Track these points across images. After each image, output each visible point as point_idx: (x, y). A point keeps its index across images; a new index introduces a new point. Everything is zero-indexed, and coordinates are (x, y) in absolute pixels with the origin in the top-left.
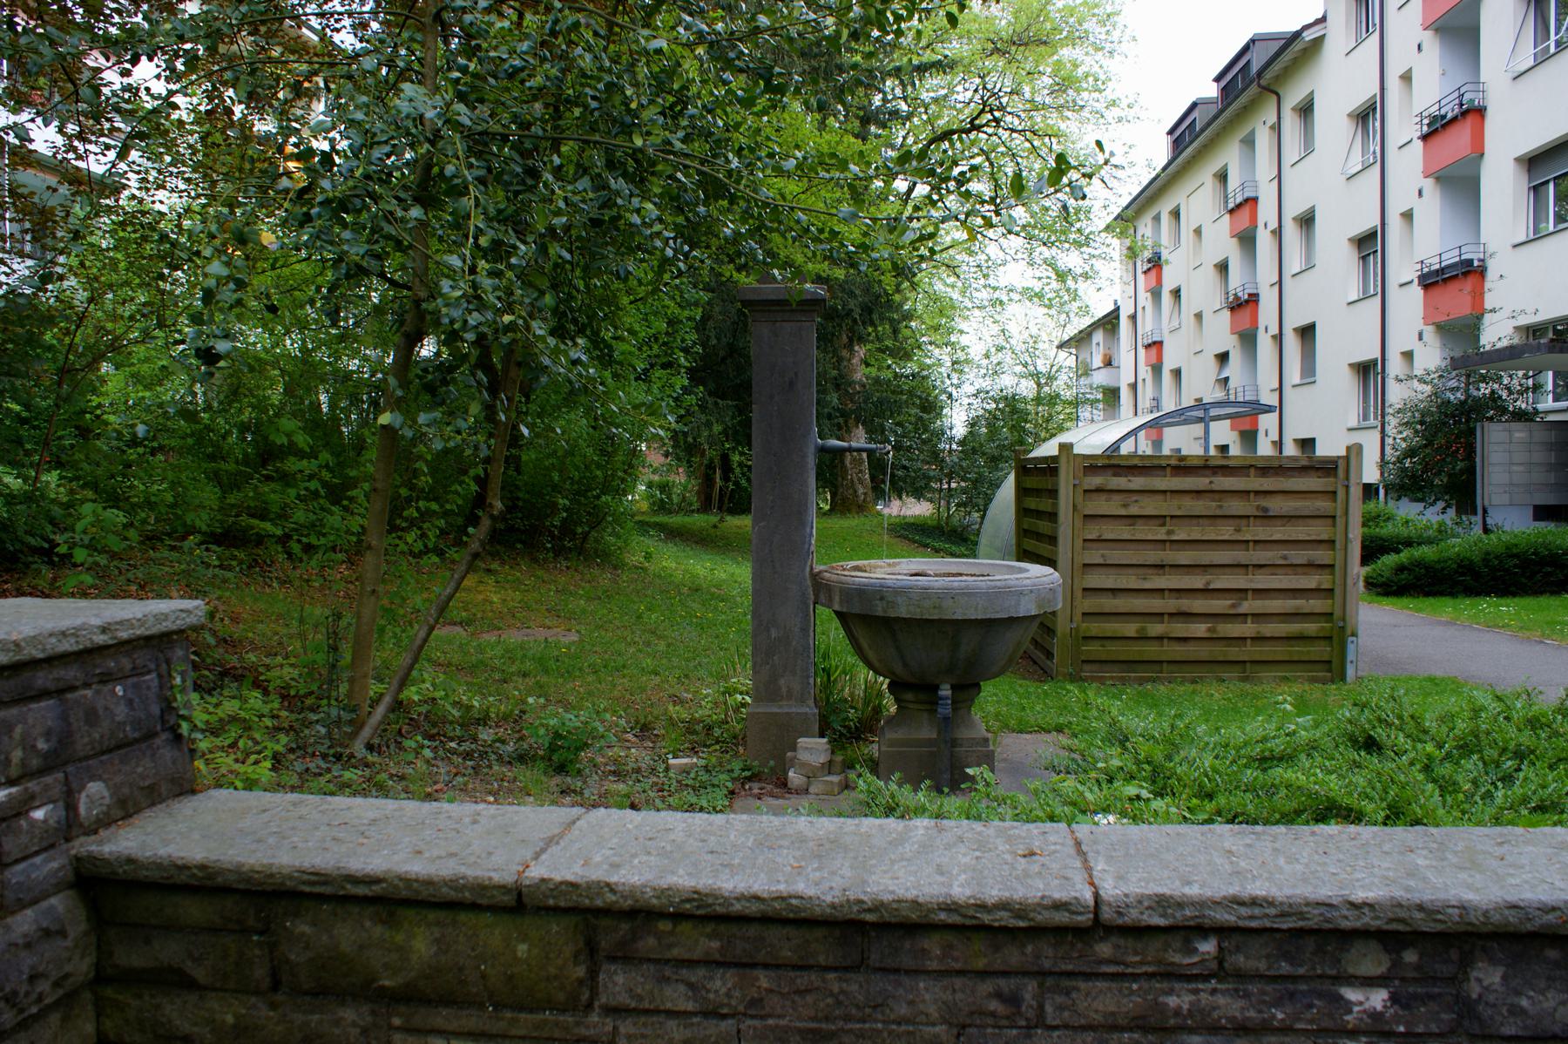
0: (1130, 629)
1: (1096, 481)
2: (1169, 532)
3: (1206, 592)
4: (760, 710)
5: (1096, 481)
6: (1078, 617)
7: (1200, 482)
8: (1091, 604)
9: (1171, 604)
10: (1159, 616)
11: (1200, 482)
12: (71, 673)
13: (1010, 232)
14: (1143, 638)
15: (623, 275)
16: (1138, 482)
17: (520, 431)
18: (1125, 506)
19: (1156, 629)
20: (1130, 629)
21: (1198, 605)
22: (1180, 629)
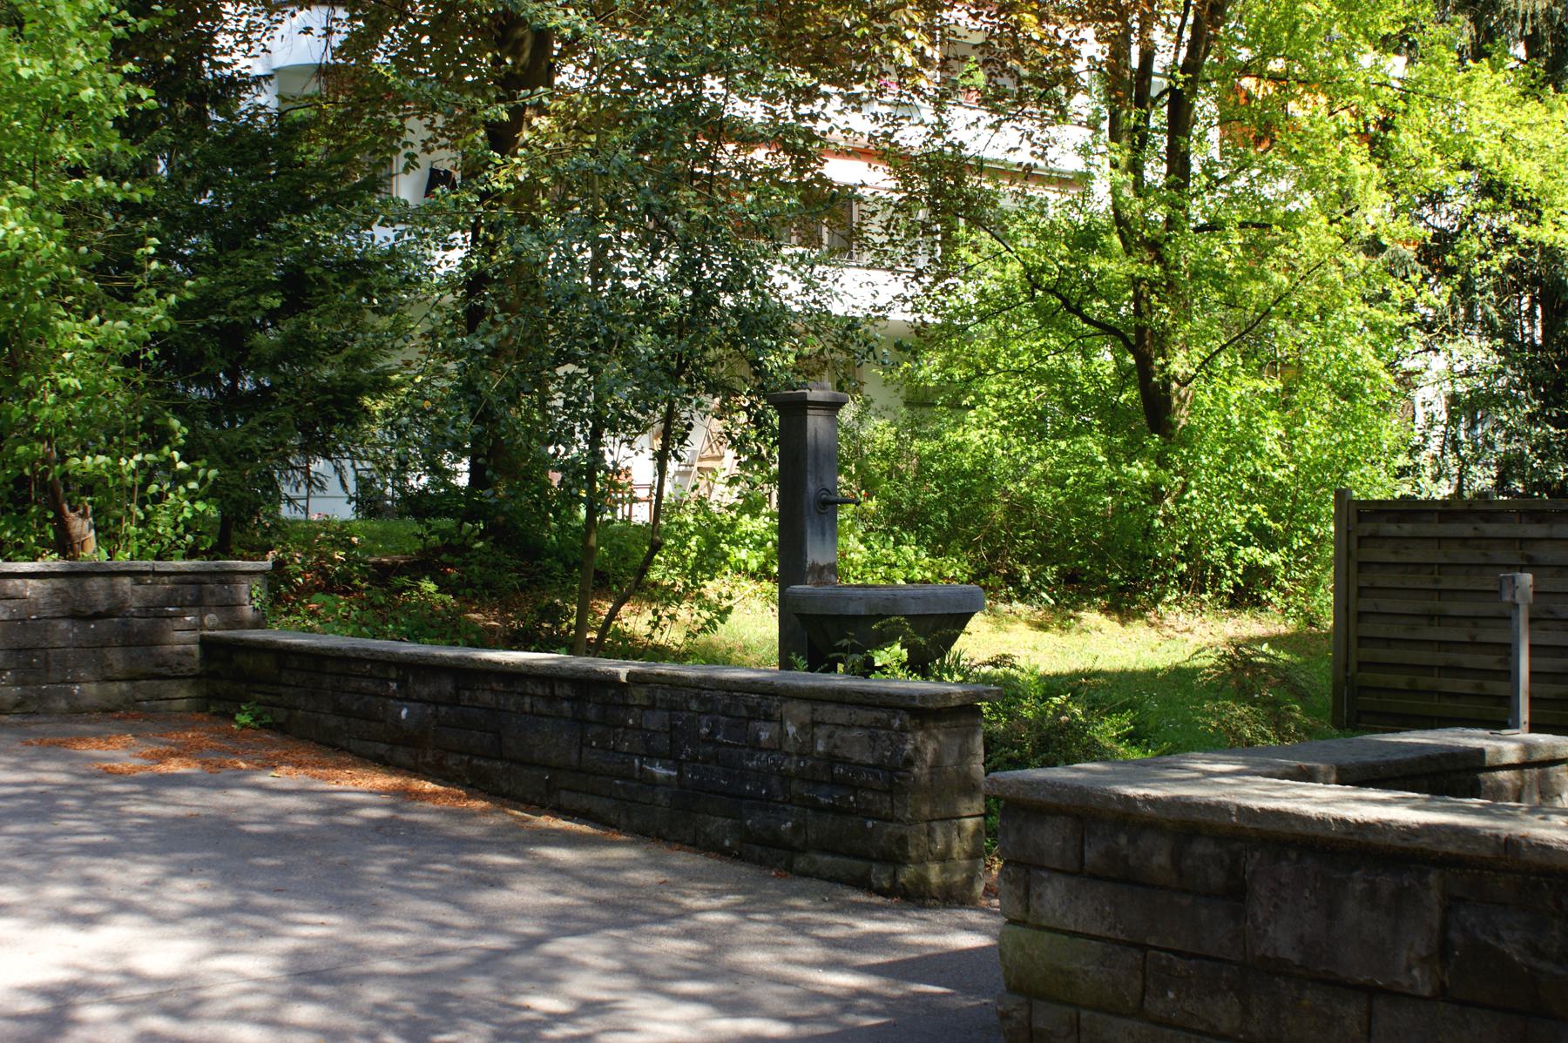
0: (1400, 681)
1: (1368, 528)
2: (1436, 581)
3: (1474, 644)
4: (898, 992)
5: (1368, 528)
6: (1353, 666)
7: (1465, 530)
8: (1367, 653)
9: (1440, 658)
10: (1427, 669)
11: (1465, 530)
12: (205, 578)
13: (23, 620)
14: (1413, 691)
15: (430, 145)
16: (1407, 529)
17: (56, 534)
18: (1396, 553)
19: (1425, 682)
20: (1400, 681)
21: (1467, 659)
22: (1449, 684)
